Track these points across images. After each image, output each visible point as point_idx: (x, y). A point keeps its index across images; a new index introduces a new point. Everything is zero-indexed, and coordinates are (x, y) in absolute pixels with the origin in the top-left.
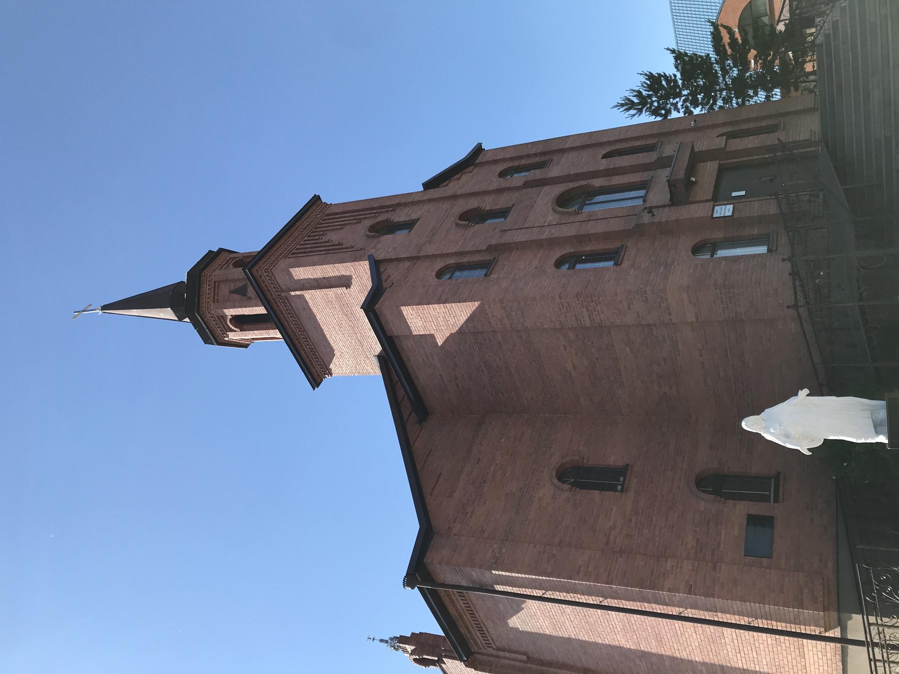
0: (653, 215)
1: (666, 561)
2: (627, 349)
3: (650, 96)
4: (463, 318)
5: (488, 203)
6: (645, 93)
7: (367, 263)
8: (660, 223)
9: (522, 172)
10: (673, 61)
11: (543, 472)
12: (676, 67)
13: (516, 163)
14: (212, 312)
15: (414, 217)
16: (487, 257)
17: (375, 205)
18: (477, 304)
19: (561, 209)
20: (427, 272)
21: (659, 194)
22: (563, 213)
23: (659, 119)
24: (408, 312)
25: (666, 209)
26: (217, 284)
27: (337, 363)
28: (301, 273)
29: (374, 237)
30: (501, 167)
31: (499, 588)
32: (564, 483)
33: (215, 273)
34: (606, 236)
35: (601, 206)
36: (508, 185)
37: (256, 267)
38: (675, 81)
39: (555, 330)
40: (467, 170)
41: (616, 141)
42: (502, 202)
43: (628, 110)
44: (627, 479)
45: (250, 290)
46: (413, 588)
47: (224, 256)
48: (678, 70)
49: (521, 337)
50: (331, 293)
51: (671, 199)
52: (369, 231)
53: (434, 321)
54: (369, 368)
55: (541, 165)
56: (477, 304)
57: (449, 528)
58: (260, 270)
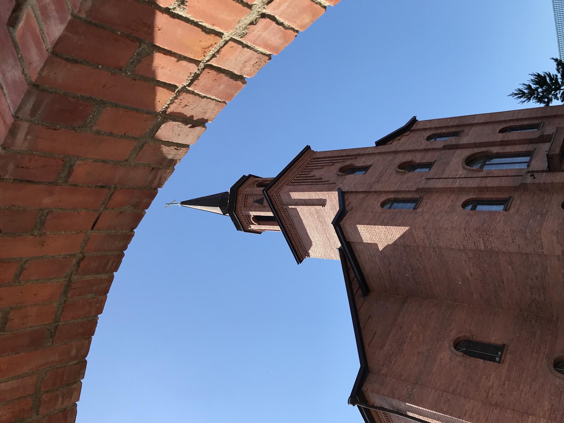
0: (534, 178)
1: (528, 417)
2: (510, 267)
3: (537, 89)
4: (397, 236)
5: (418, 158)
6: (533, 86)
7: (337, 193)
8: (539, 184)
9: (443, 137)
10: (556, 66)
11: (444, 341)
12: (558, 70)
13: (439, 131)
14: (243, 212)
15: (368, 163)
16: (417, 196)
17: (344, 154)
18: (407, 228)
19: (468, 167)
20: (375, 202)
21: (539, 162)
22: (469, 170)
23: (542, 105)
24: (361, 228)
25: (544, 174)
26: (246, 196)
27: (313, 250)
28: (295, 195)
29: (342, 175)
30: (428, 133)
31: (410, 414)
32: (458, 350)
33: (246, 189)
34: (500, 189)
35: (495, 167)
36: (432, 147)
37: (270, 190)
38: (557, 79)
39: (460, 250)
40: (406, 134)
41: (511, 120)
42: (428, 157)
43: (520, 97)
44: (504, 354)
45: (265, 201)
46: (354, 406)
47: (252, 179)
48: (559, 72)
49: (436, 252)
50: (312, 208)
51: (549, 167)
52: (339, 171)
53: (378, 236)
54: (333, 255)
55: (456, 134)
56: (407, 228)
57: (379, 370)
58: (272, 192)
